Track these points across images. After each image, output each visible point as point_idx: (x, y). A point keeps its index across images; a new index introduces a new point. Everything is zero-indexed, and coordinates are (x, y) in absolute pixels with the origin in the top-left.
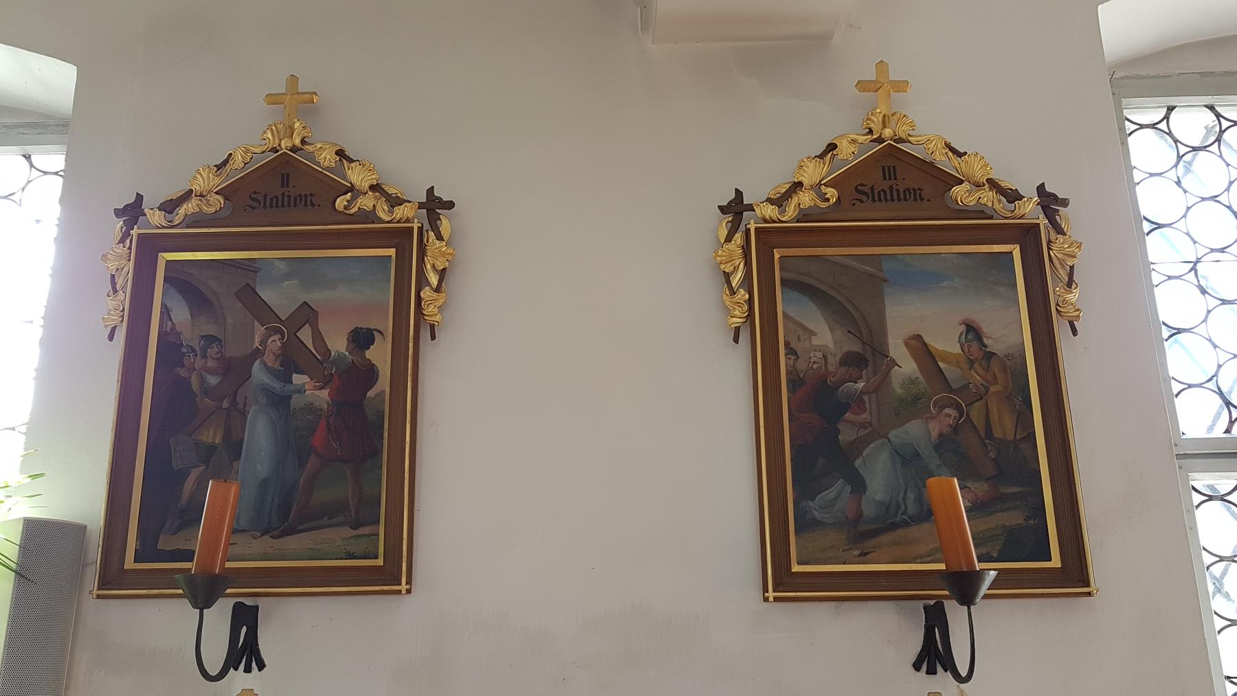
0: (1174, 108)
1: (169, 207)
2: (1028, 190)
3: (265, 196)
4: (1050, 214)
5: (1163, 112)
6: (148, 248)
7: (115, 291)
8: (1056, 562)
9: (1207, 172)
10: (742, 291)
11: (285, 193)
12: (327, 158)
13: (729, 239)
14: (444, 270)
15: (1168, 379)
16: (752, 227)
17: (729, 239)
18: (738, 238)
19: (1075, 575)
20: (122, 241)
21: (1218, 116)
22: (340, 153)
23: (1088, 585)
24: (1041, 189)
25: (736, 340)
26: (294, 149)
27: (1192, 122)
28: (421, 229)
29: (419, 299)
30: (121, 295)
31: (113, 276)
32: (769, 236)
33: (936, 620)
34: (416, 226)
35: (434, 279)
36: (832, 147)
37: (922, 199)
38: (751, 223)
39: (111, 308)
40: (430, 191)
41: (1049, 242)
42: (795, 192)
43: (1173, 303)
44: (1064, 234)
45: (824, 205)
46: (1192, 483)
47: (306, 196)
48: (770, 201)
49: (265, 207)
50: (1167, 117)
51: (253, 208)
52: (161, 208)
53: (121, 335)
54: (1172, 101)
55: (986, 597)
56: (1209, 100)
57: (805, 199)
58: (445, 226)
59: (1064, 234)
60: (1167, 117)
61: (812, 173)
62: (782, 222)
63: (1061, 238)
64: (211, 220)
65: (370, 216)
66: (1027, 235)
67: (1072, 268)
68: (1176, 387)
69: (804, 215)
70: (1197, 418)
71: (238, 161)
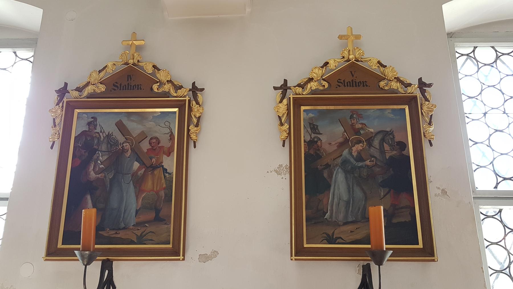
0: (477, 47)
1: (79, 89)
2: (415, 83)
3: (121, 85)
4: (423, 92)
5: (472, 49)
6: (70, 107)
7: (55, 126)
8: (421, 246)
9: (490, 75)
10: (286, 124)
11: (130, 83)
12: (149, 69)
13: (281, 102)
14: (199, 117)
15: (471, 163)
16: (291, 96)
17: (281, 102)
18: (61, 104)
19: (428, 252)
20: (58, 104)
21: (496, 51)
22: (154, 66)
23: (434, 256)
24: (420, 80)
25: (284, 146)
26: (134, 64)
27: (485, 53)
28: (189, 101)
29: (189, 130)
30: (58, 128)
31: (54, 119)
32: (298, 102)
33: (366, 273)
34: (187, 99)
35: (195, 120)
36: (326, 64)
37: (367, 86)
38: (290, 94)
39: (49, 133)
40: (194, 83)
41: (421, 105)
42: (309, 82)
43: (474, 131)
44: (429, 101)
45: (321, 88)
46: (481, 210)
47: (138, 85)
48: (299, 85)
49: (120, 89)
50: (474, 51)
51: (115, 90)
52: (76, 90)
53: (57, 147)
54: (475, 44)
55: (388, 260)
56: (492, 44)
57: (313, 85)
58: (200, 99)
59: (429, 101)
60: (474, 51)
61: (318, 73)
62: (303, 95)
63: (427, 103)
64: (101, 95)
65: (167, 94)
66: (411, 101)
67: (431, 116)
68: (474, 167)
69: (313, 92)
70: (484, 181)
71: (332, 65)
